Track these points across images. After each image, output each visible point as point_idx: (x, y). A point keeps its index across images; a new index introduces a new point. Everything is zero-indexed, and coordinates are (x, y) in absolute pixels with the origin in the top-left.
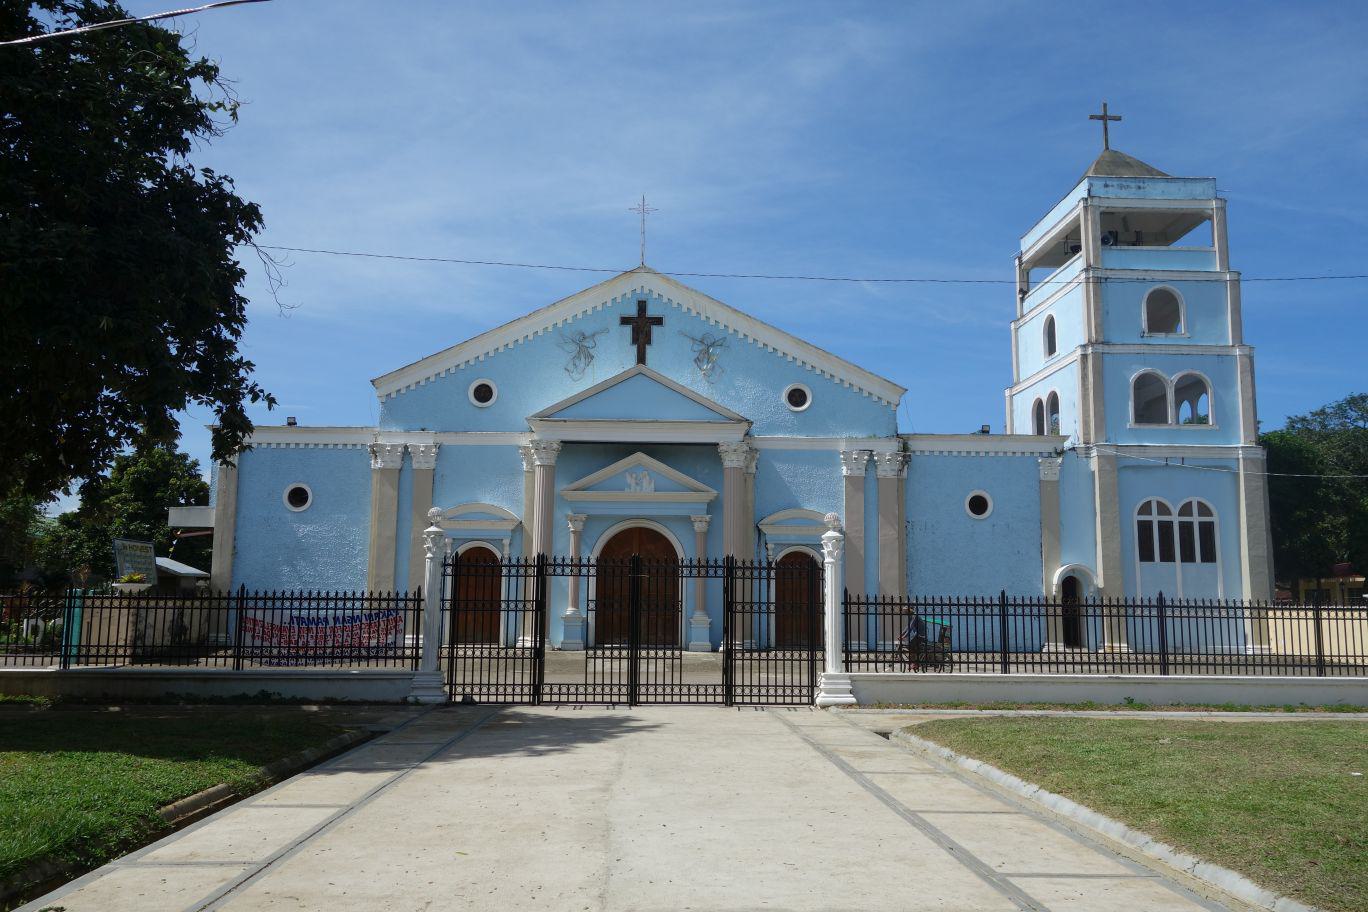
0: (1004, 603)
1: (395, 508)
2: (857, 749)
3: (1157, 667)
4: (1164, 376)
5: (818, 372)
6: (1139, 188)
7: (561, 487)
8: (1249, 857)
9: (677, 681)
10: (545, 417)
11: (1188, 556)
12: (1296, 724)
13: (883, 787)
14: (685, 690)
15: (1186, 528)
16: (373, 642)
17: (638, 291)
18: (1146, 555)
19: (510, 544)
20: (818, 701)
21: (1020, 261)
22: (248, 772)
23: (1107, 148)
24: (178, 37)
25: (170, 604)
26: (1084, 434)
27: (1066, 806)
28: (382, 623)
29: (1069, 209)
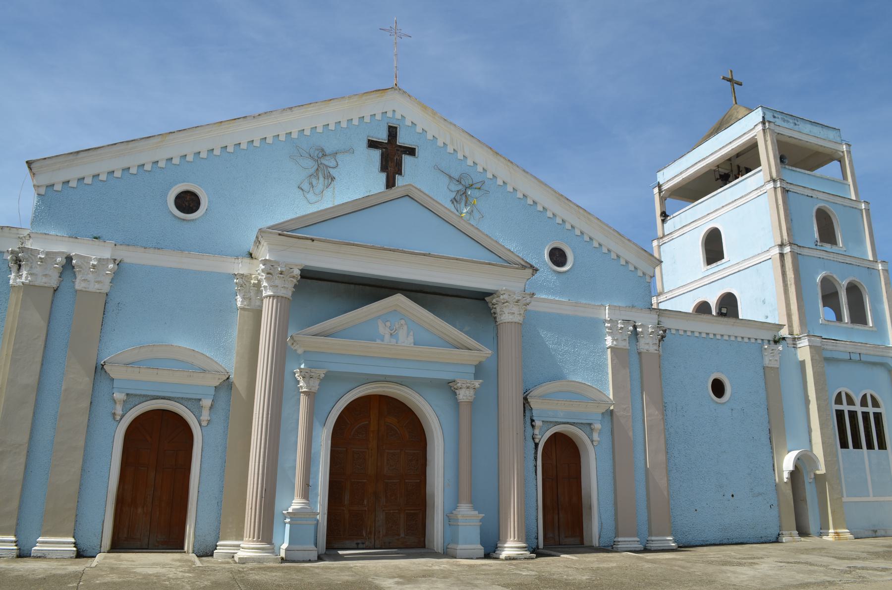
1: (41, 343)
11: (857, 445)
15: (866, 415)
17: (390, 114)
18: (844, 445)
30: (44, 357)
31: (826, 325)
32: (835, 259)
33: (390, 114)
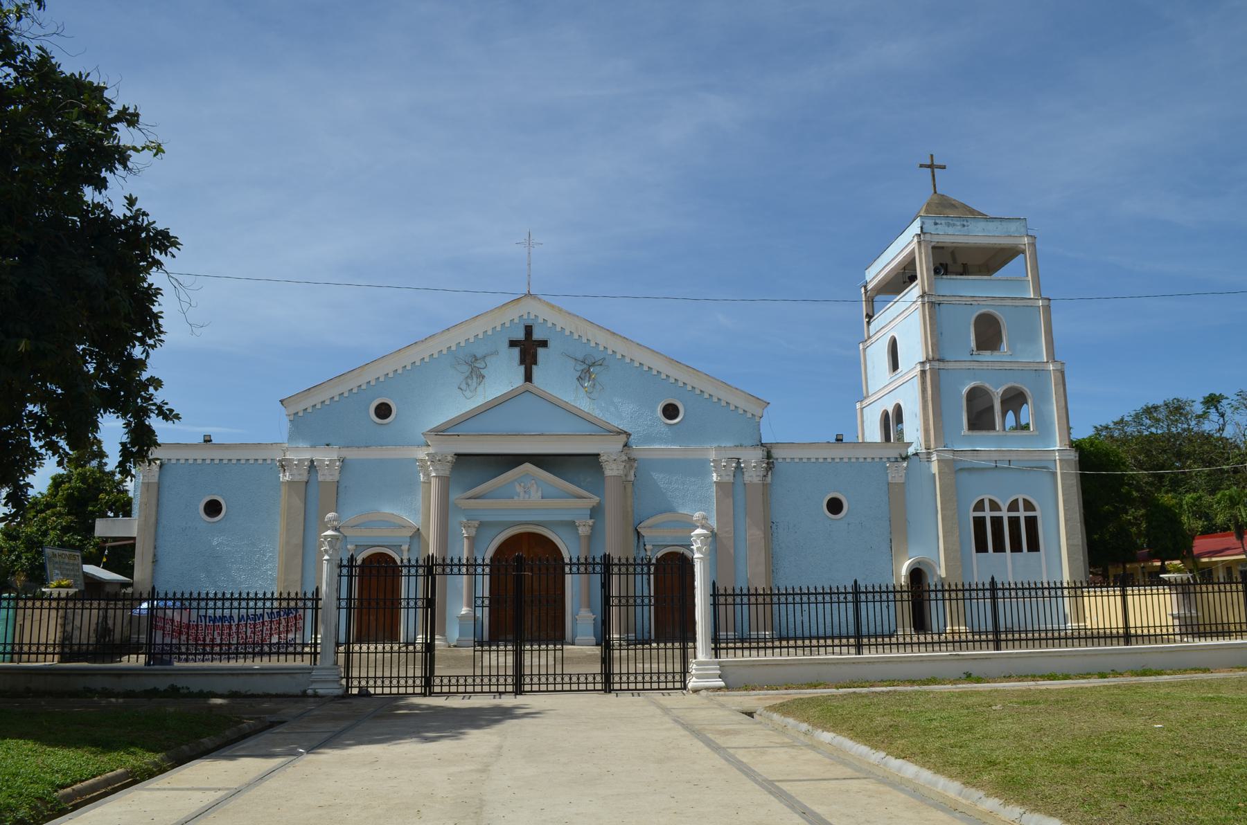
0: (856, 591)
2: (723, 728)
3: (991, 644)
4: (991, 388)
5: (689, 388)
6: (964, 226)
7: (455, 496)
8: (1068, 805)
10: (440, 432)
11: (1016, 548)
12: (1108, 688)
13: (745, 760)
14: (567, 679)
15: (1014, 522)
16: (275, 639)
17: (525, 317)
18: (981, 547)
19: (409, 550)
20: (690, 685)
21: (866, 290)
22: (149, 758)
23: (935, 192)
24: (103, 89)
25: (95, 604)
26: (925, 441)
27: (909, 770)
28: (283, 621)
29: (905, 244)
30: (304, 526)
31: (969, 436)
32: (990, 368)
33: (525, 317)
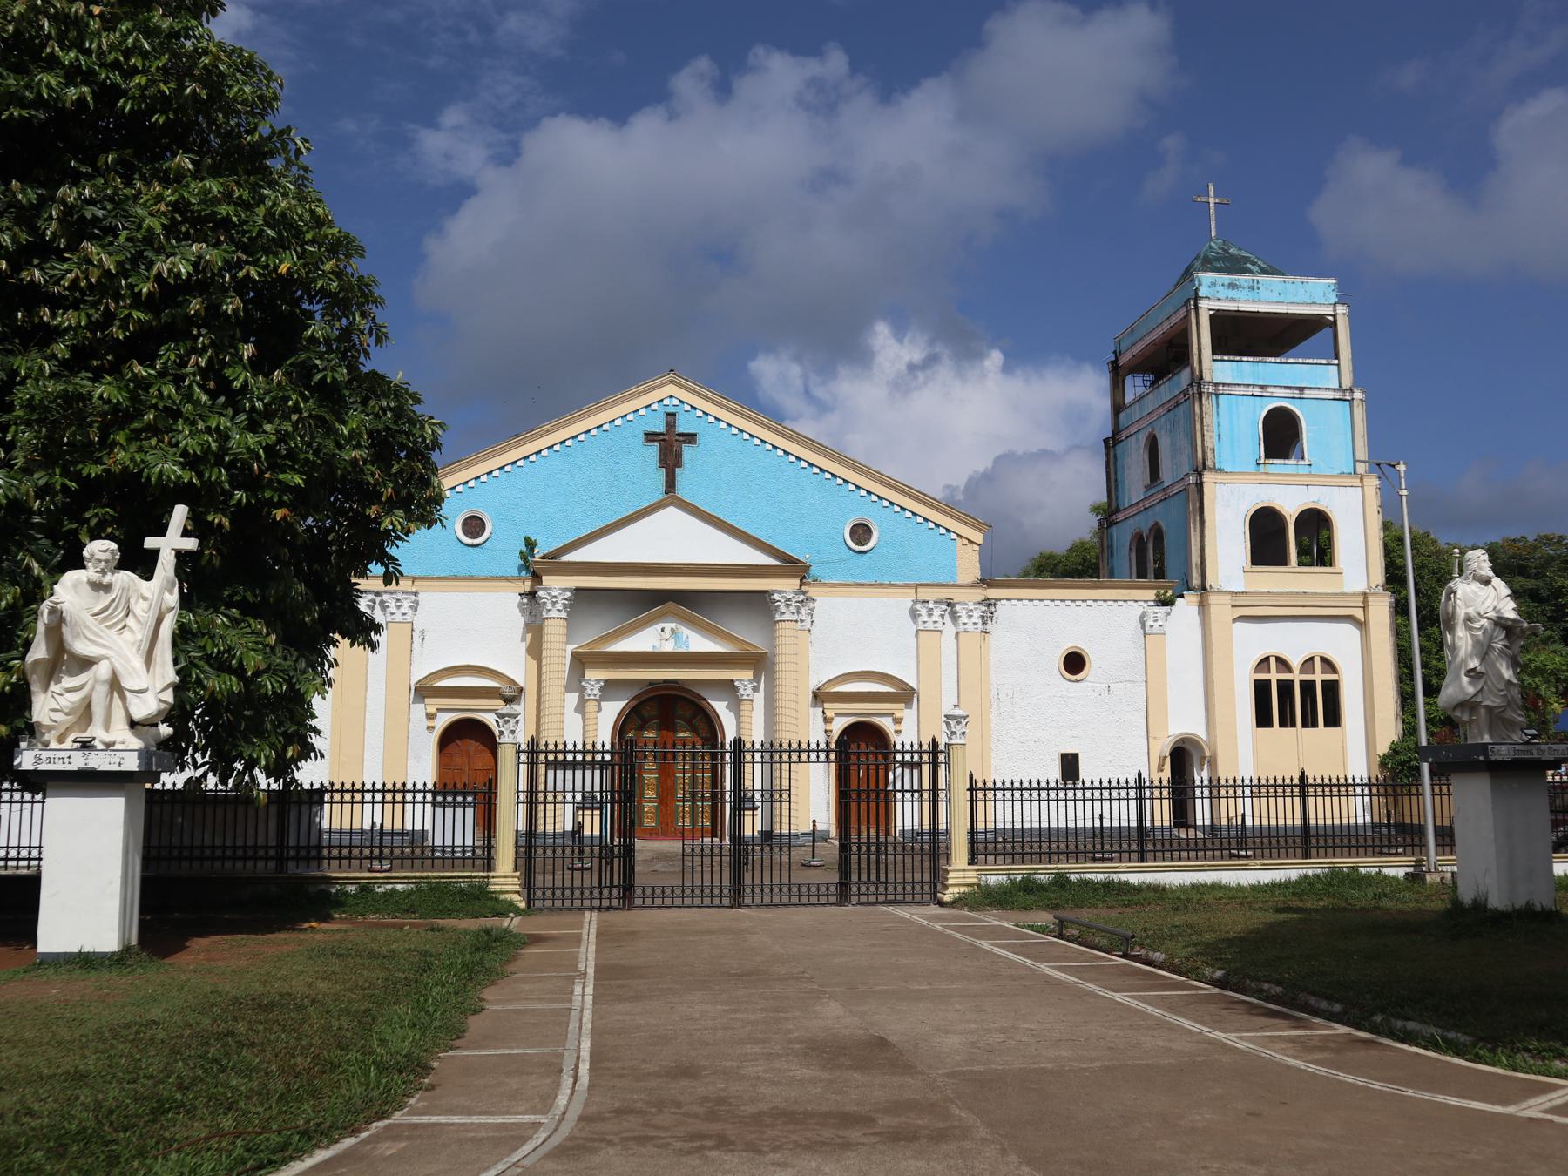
9: (785, 880)
14: (795, 889)
15: (1308, 687)
18: (1263, 719)
